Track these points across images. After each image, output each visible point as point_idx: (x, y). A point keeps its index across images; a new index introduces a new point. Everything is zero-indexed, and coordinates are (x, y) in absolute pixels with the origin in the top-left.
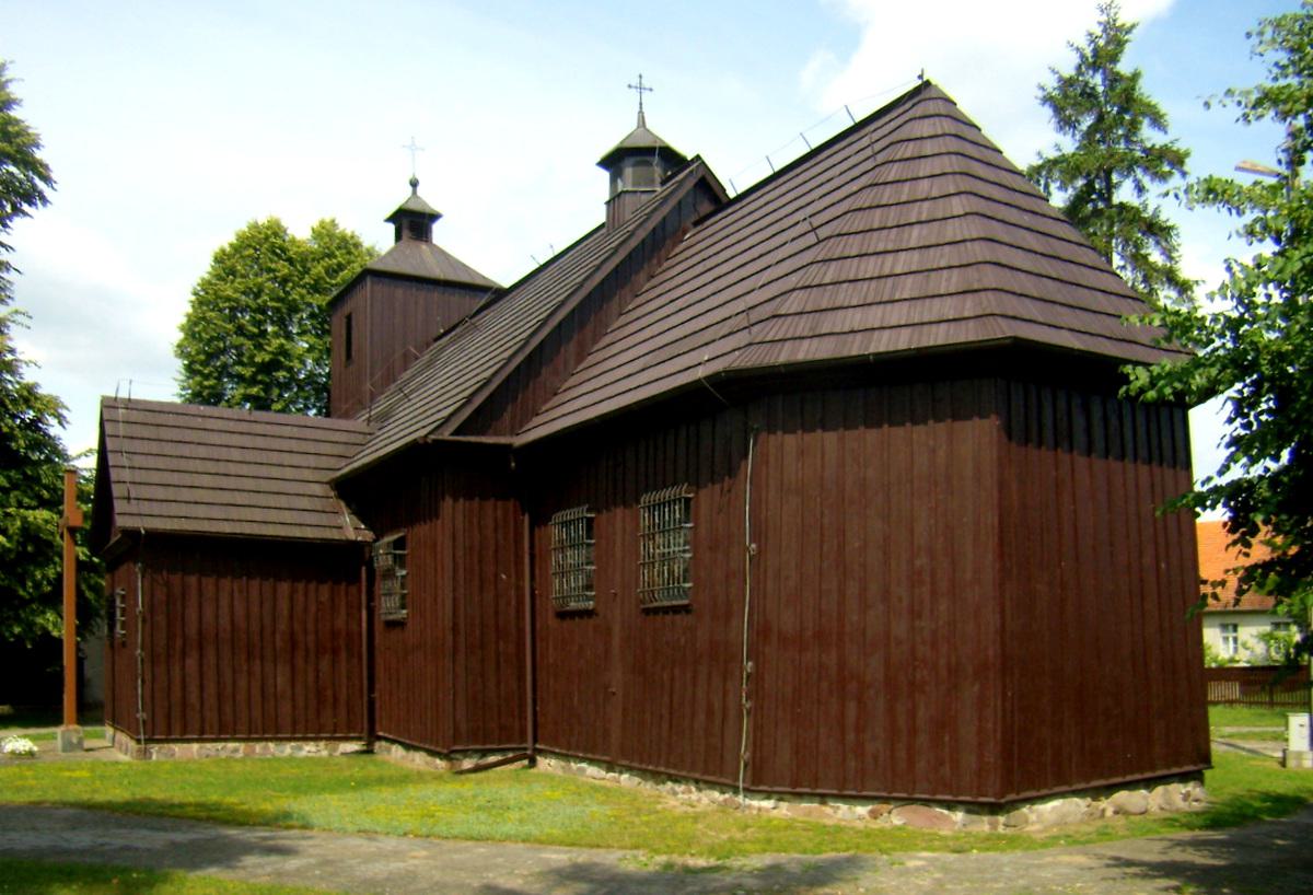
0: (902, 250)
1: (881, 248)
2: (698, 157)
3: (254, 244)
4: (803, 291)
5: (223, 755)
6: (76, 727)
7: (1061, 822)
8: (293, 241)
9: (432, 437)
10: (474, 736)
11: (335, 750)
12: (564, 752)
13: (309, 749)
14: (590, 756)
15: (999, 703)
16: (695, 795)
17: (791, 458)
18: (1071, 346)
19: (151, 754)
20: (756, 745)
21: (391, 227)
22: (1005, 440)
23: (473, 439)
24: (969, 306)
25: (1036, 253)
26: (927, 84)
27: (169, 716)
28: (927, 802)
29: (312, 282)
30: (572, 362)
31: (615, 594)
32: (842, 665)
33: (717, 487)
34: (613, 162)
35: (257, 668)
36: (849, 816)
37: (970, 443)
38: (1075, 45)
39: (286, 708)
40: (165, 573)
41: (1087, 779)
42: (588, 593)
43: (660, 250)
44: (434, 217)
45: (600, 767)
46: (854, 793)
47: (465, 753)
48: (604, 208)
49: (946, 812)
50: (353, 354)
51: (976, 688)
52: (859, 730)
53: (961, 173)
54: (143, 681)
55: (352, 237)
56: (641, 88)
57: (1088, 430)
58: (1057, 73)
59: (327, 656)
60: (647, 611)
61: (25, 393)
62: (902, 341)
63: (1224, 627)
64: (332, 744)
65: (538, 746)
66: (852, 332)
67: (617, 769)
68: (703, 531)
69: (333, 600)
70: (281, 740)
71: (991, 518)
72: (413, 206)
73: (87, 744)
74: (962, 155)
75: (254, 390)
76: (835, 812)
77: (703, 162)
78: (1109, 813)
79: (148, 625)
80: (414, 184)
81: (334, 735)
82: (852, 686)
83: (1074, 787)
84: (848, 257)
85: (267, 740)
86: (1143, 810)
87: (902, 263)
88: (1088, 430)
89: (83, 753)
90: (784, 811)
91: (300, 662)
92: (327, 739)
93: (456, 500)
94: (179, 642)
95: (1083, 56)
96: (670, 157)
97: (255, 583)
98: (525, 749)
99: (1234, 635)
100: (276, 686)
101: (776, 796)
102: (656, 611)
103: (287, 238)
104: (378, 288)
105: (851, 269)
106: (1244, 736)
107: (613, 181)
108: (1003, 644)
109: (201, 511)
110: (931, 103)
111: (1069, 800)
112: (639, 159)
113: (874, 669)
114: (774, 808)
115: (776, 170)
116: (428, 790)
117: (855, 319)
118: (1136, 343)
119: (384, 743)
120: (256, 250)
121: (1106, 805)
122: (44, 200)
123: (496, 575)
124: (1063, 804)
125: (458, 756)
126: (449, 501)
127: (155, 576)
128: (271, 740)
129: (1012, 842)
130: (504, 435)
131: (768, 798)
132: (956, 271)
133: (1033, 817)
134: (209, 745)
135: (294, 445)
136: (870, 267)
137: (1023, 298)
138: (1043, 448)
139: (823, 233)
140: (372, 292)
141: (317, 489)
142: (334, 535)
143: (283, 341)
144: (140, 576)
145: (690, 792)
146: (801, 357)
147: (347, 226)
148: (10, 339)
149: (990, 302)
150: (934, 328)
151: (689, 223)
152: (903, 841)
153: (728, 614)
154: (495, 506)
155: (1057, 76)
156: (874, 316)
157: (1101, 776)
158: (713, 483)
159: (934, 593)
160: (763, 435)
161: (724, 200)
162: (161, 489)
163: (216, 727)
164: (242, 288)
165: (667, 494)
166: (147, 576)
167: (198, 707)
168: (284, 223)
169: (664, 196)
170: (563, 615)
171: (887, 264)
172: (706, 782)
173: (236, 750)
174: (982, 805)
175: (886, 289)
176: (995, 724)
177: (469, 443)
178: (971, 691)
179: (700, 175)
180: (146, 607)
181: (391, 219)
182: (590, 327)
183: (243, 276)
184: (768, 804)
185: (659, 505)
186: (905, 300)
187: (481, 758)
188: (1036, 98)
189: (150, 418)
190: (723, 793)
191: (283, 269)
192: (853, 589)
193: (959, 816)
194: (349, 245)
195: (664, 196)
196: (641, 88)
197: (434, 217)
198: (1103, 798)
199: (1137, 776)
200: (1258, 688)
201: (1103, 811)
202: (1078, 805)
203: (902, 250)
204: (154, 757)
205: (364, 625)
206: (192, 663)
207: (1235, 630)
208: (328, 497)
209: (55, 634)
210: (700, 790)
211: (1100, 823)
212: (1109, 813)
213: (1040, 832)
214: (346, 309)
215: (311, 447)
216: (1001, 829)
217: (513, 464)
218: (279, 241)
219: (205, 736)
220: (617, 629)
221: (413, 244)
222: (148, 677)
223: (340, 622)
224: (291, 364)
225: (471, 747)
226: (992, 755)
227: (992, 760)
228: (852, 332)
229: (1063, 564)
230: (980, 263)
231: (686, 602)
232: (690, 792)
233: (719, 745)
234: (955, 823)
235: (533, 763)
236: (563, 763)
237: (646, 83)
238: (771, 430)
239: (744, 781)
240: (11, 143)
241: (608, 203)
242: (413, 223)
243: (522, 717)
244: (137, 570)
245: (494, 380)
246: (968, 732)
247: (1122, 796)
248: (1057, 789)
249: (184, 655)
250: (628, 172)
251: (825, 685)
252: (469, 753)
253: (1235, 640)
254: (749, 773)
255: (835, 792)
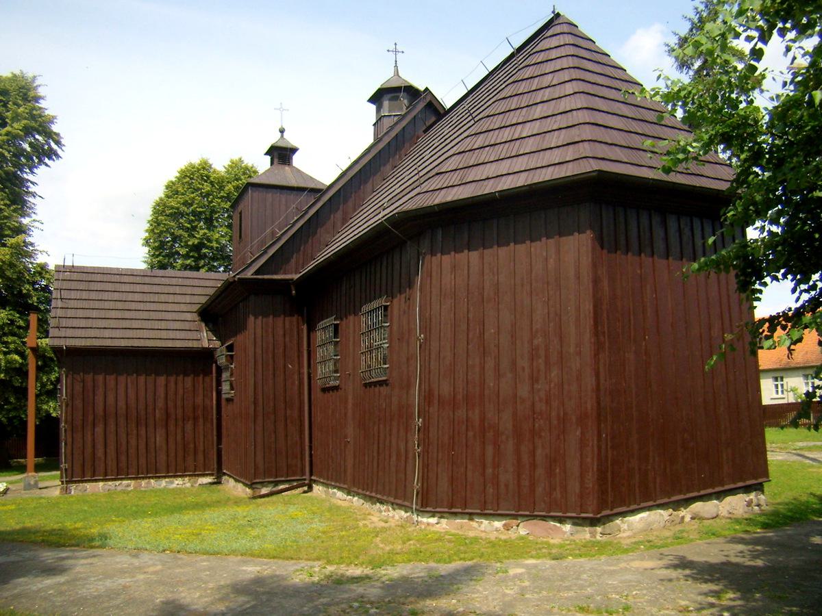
0: (528, 121)
1: (514, 121)
2: (427, 89)
3: (188, 175)
4: (459, 155)
5: (119, 488)
6: (34, 474)
7: (648, 529)
8: (215, 171)
9: (238, 276)
10: (267, 473)
11: (196, 482)
12: (325, 481)
13: (178, 482)
14: (338, 484)
15: (595, 442)
16: (391, 513)
17: (446, 272)
18: (646, 176)
19: (71, 490)
20: (424, 478)
21: (268, 158)
22: (598, 248)
23: (266, 277)
24: (570, 153)
25: (628, 117)
26: (558, 15)
27: (83, 466)
28: (544, 518)
29: (225, 195)
30: (339, 224)
31: (349, 375)
32: (483, 419)
33: (403, 296)
34: (376, 99)
35: (143, 432)
36: (489, 529)
37: (571, 253)
38: (688, 17)
39: (162, 457)
40: (81, 374)
41: (669, 495)
42: (335, 375)
43: (401, 150)
44: (294, 150)
45: (343, 492)
46: (491, 512)
47: (263, 484)
48: (373, 127)
49: (558, 525)
50: (243, 236)
51: (578, 433)
52: (496, 466)
53: (574, 68)
54: (66, 444)
55: (252, 167)
56: (396, 51)
57: (666, 239)
58: (678, 34)
59: (190, 422)
60: (366, 385)
61: (39, 269)
62: (521, 181)
63: (776, 379)
64: (193, 479)
65: (313, 478)
66: (488, 179)
67: (352, 494)
68: (395, 328)
69: (194, 386)
70: (159, 477)
71: (588, 307)
72: (281, 144)
73: (41, 485)
74: (577, 56)
75: (188, 262)
76: (480, 526)
77: (430, 92)
78: (687, 519)
79: (70, 408)
80: (282, 131)
81: (195, 472)
82: (490, 435)
83: (659, 502)
84: (492, 130)
85: (149, 478)
86: (715, 515)
87: (527, 130)
88: (666, 239)
89: (38, 490)
90: (444, 526)
91: (172, 428)
92: (190, 476)
93: (256, 318)
94: (91, 418)
95: (693, 23)
96: (411, 92)
97: (142, 379)
98: (305, 479)
99: (782, 383)
100: (155, 443)
101: (439, 515)
102: (370, 384)
103: (211, 171)
104: (255, 194)
105: (492, 138)
106: (810, 449)
107: (378, 110)
108: (598, 398)
109: (107, 333)
110: (559, 26)
111: (653, 512)
112: (393, 95)
113: (506, 422)
114: (437, 524)
115: (469, 89)
116: (241, 511)
117: (490, 170)
118: (702, 176)
119: (226, 477)
120: (192, 179)
121: (686, 513)
122: (58, 156)
123: (285, 366)
124: (649, 516)
125: (259, 486)
126: (252, 318)
127: (75, 376)
128: (152, 478)
129: (602, 548)
130: (292, 273)
131: (433, 516)
132: (563, 131)
133: (625, 526)
134: (110, 483)
135: (178, 290)
136: (506, 134)
137: (613, 147)
138: (630, 254)
139: (476, 119)
140: (251, 194)
141: (189, 316)
142: (195, 345)
143: (206, 231)
144: (64, 376)
145: (389, 511)
146: (449, 199)
147: (249, 161)
148: (30, 236)
149: (585, 149)
150: (544, 170)
151: (421, 132)
152: (517, 550)
153: (409, 386)
154: (284, 320)
155: (677, 36)
156: (504, 167)
157: (680, 492)
158: (400, 294)
159: (547, 362)
160: (428, 257)
161: (442, 112)
162: (84, 321)
163: (145, 471)
164: (182, 201)
165: (375, 304)
166: (70, 376)
167: (103, 458)
168: (210, 162)
169: (408, 113)
170: (325, 390)
171: (518, 132)
172: (397, 504)
173: (128, 486)
174: (584, 518)
175: (515, 148)
176: (593, 459)
177: (263, 279)
178: (575, 434)
179: (428, 101)
180: (69, 397)
181: (267, 154)
182: (350, 204)
183: (183, 194)
184: (433, 520)
185: (370, 311)
186: (526, 153)
187: (274, 487)
188: (666, 51)
189: (85, 277)
190: (406, 512)
191: (207, 187)
192: (490, 363)
193: (567, 527)
194: (249, 171)
195: (408, 113)
196: (396, 51)
197: (294, 150)
198: (682, 509)
199: (710, 491)
200: (431, 514)
201: (683, 518)
202: (661, 515)
203: (528, 121)
204: (73, 492)
205: (214, 402)
206: (99, 429)
207: (782, 379)
208: (194, 321)
209: (54, 415)
210: (394, 509)
211: (679, 528)
212: (687, 519)
213: (629, 537)
214: (240, 208)
215: (189, 290)
216: (598, 537)
217: (294, 292)
218: (206, 172)
219: (107, 477)
220: (350, 397)
221: (281, 167)
222: (69, 440)
223: (199, 400)
224: (211, 245)
225: (267, 480)
226: (591, 480)
227: (591, 485)
228: (488, 179)
229: (647, 337)
230: (580, 124)
231: (384, 378)
232: (389, 511)
233: (403, 479)
234: (565, 533)
235: (310, 489)
236: (325, 489)
237: (399, 48)
238: (433, 254)
239: (417, 504)
240: (36, 121)
241: (374, 125)
242: (281, 154)
243: (302, 459)
244: (63, 372)
245: (283, 238)
246: (573, 465)
247: (697, 506)
248: (643, 505)
249: (94, 425)
250: (386, 103)
251: (471, 434)
252: (265, 483)
253: (782, 385)
254: (419, 502)
255: (479, 511)
